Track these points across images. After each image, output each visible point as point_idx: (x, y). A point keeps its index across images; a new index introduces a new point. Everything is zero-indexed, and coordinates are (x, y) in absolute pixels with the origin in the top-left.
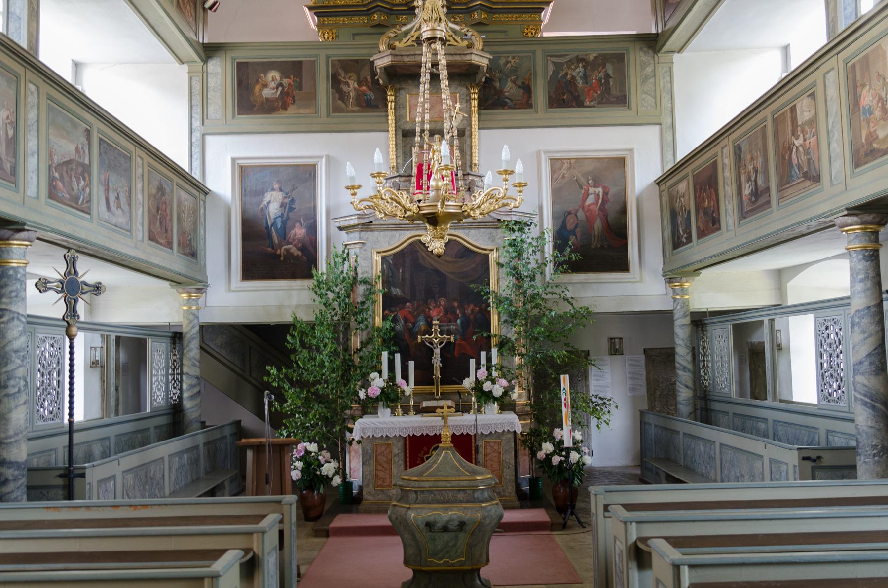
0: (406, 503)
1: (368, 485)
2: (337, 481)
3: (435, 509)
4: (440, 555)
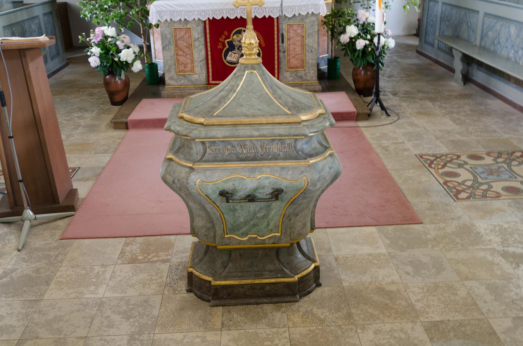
0: (187, 160)
1: (169, 70)
2: (138, 66)
3: (234, 171)
4: (244, 230)
